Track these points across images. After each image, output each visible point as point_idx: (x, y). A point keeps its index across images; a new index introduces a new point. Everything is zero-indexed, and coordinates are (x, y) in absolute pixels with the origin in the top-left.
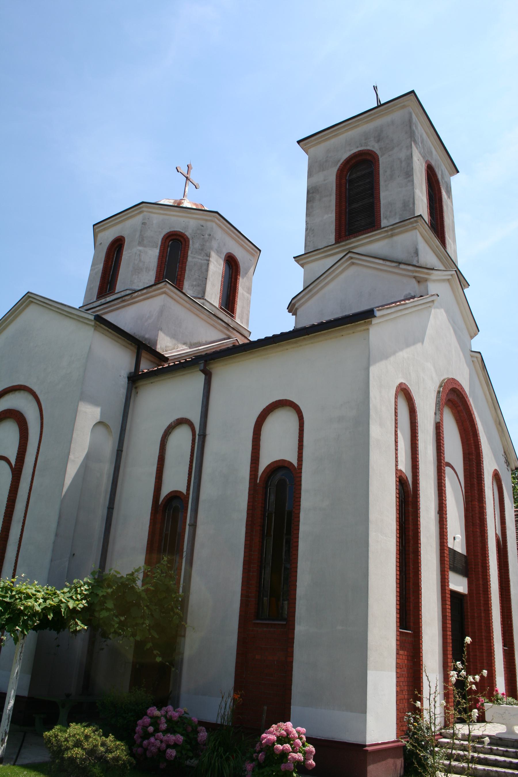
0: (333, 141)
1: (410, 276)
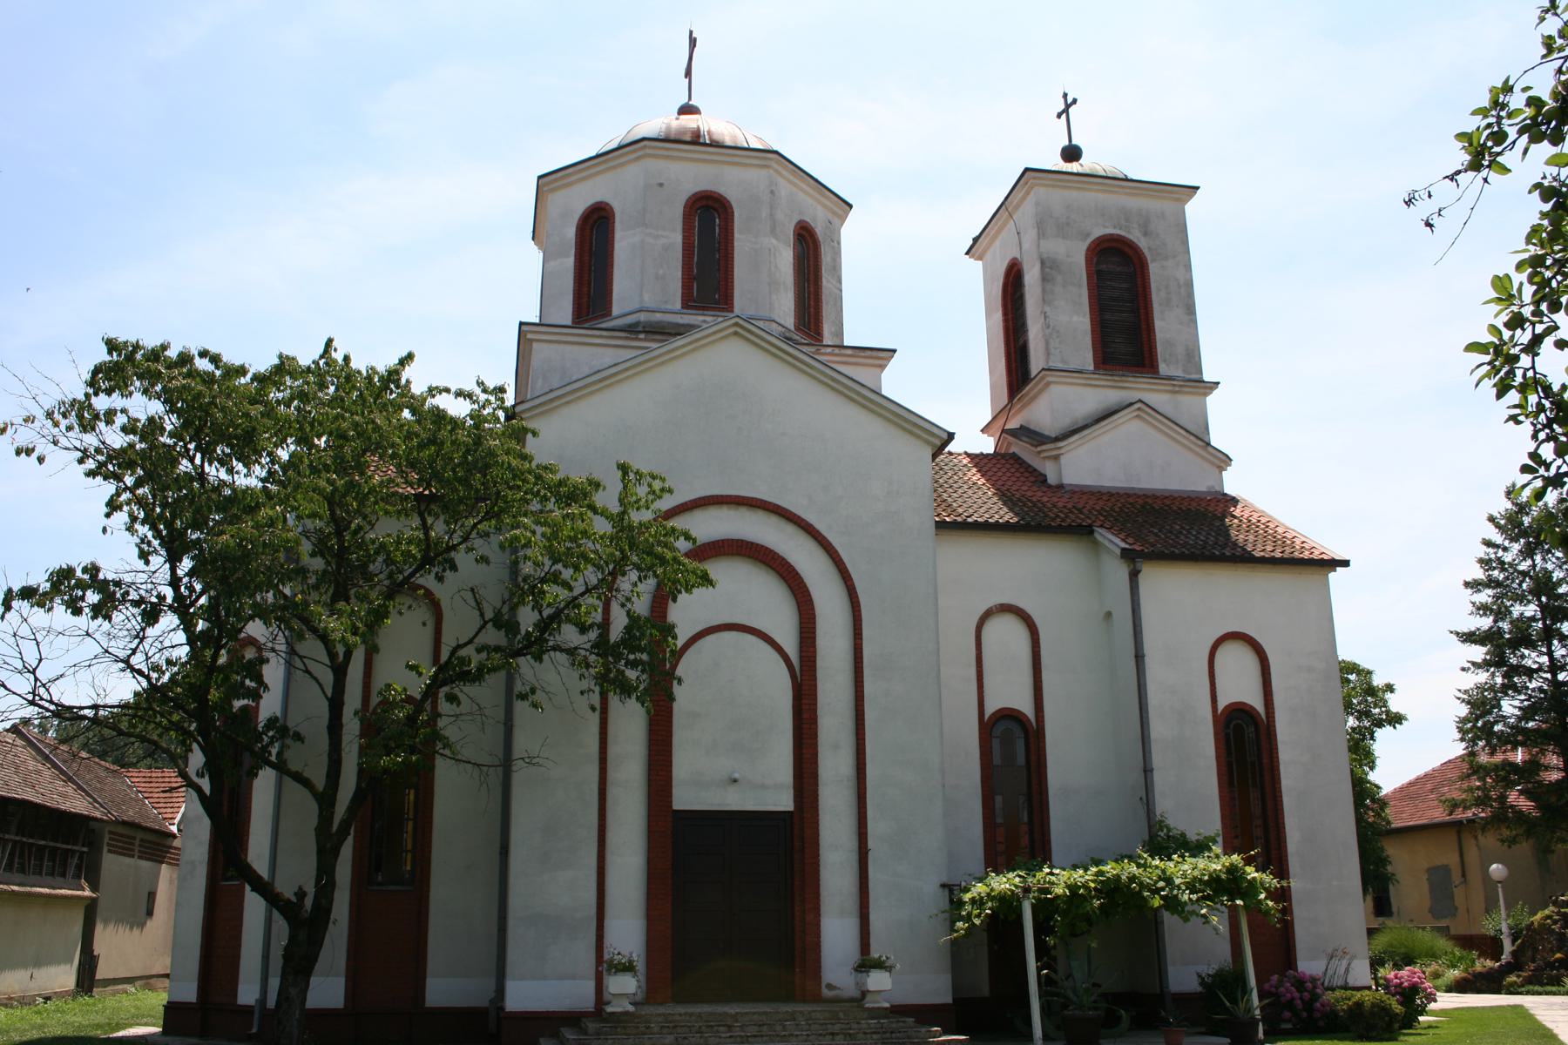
0: (1075, 194)
1: (1213, 464)
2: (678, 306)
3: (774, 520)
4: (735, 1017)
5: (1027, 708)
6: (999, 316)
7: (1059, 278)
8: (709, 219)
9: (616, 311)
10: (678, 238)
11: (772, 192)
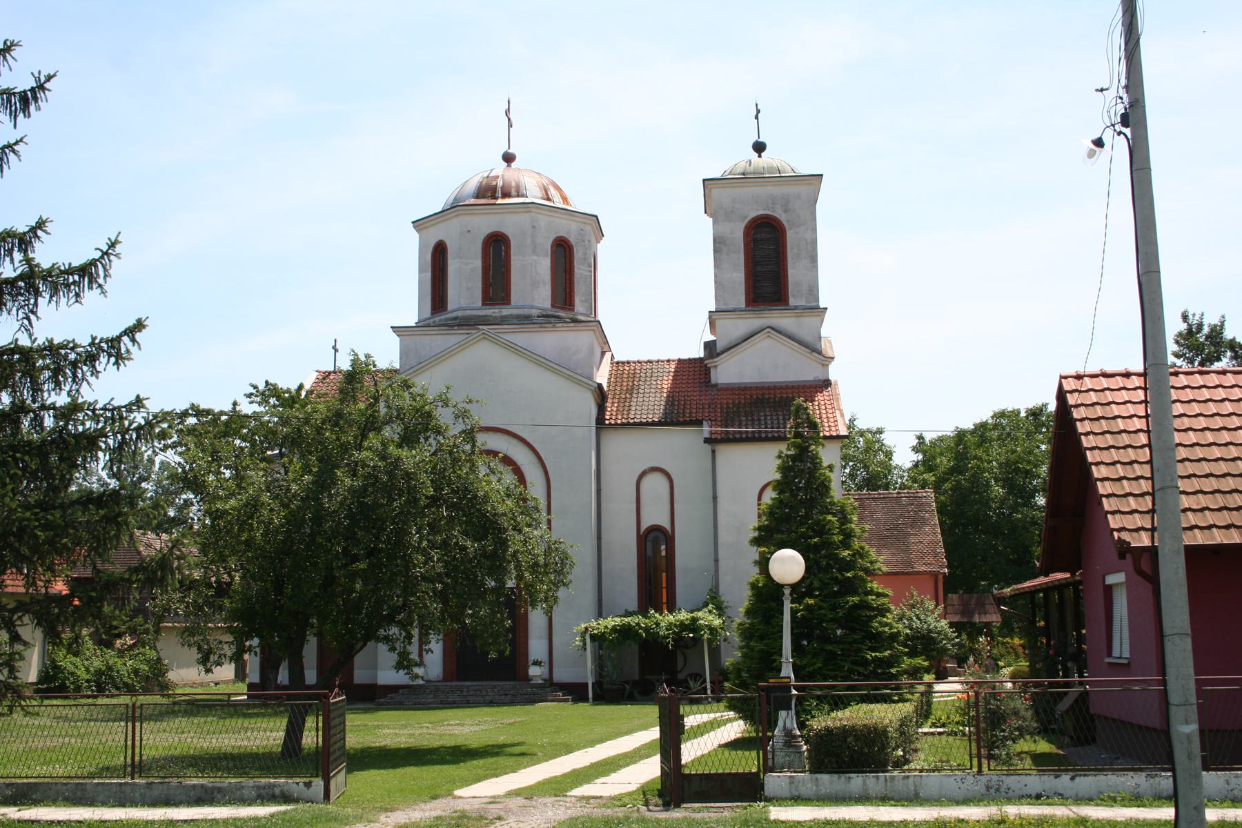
2: (480, 304)
3: (506, 437)
4: (467, 687)
5: (667, 526)
6: (429, 275)
7: (725, 250)
8: (496, 249)
9: (450, 307)
10: (478, 263)
11: (534, 227)
